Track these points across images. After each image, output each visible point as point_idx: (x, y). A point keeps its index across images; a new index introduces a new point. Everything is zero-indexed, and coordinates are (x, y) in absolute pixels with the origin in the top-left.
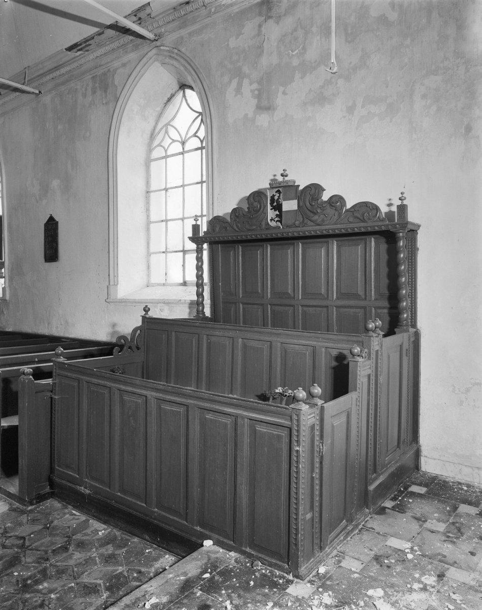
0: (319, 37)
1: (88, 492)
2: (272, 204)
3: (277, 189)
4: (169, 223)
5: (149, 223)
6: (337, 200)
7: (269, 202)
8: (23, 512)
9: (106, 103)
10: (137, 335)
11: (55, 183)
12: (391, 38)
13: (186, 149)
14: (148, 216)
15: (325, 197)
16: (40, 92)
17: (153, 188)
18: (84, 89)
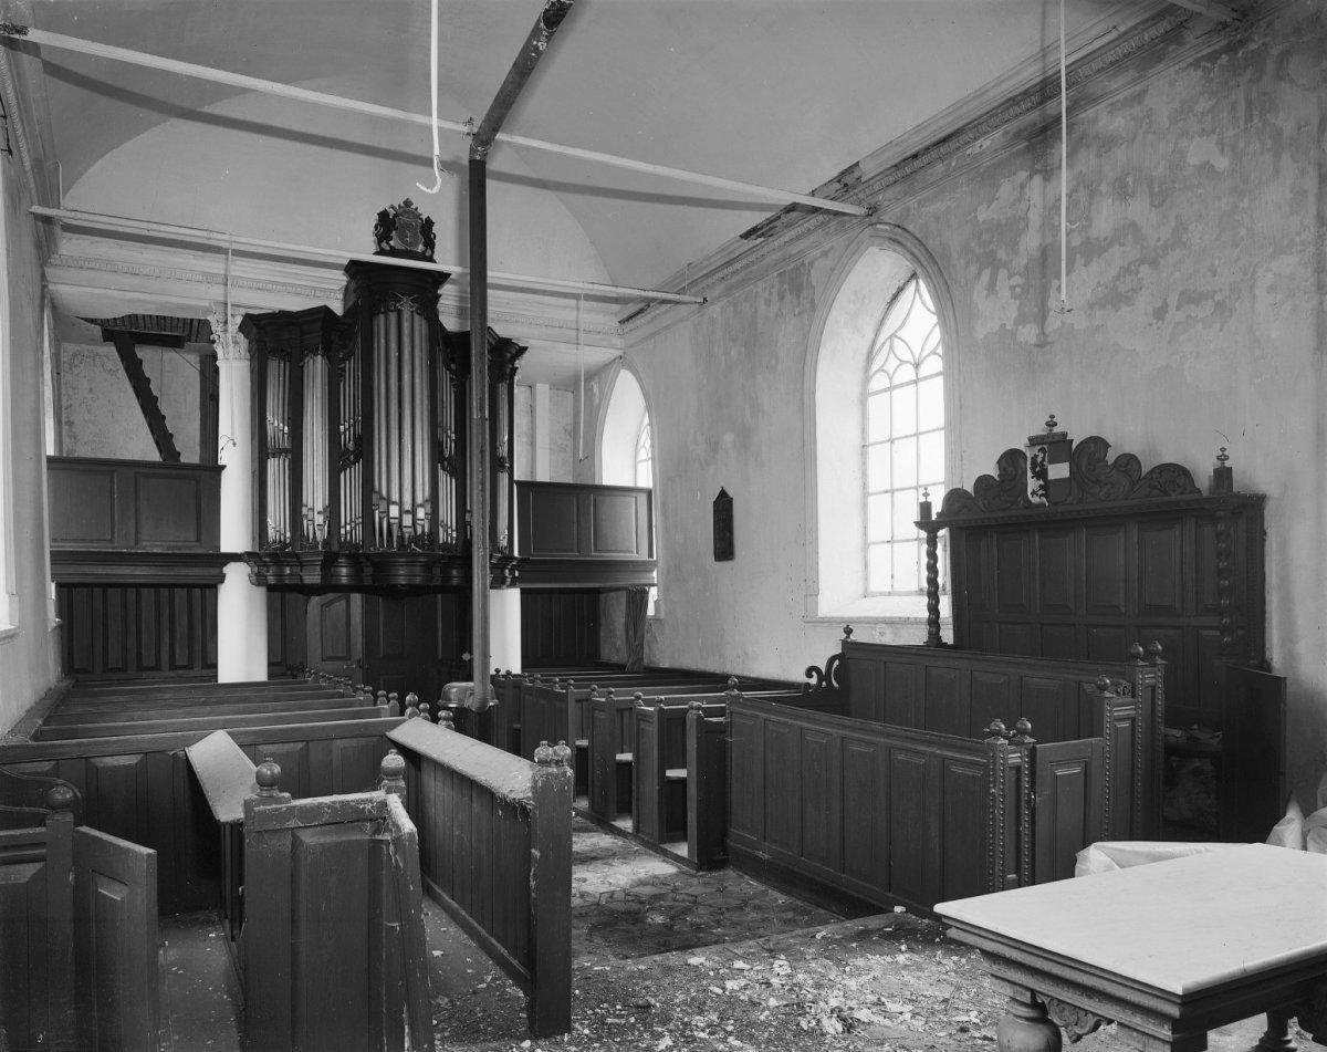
0: (1110, 200)
1: (766, 857)
2: (1033, 469)
3: (1039, 447)
4: (896, 494)
5: (865, 495)
6: (1129, 461)
7: (1029, 466)
8: (693, 876)
9: (800, 314)
10: (835, 666)
11: (728, 439)
12: (1220, 198)
13: (921, 375)
14: (865, 485)
15: (1111, 457)
16: (705, 300)
17: (871, 440)
18: (767, 293)
